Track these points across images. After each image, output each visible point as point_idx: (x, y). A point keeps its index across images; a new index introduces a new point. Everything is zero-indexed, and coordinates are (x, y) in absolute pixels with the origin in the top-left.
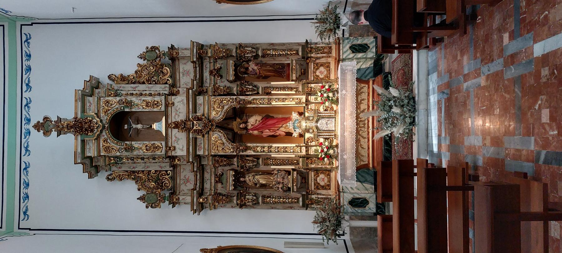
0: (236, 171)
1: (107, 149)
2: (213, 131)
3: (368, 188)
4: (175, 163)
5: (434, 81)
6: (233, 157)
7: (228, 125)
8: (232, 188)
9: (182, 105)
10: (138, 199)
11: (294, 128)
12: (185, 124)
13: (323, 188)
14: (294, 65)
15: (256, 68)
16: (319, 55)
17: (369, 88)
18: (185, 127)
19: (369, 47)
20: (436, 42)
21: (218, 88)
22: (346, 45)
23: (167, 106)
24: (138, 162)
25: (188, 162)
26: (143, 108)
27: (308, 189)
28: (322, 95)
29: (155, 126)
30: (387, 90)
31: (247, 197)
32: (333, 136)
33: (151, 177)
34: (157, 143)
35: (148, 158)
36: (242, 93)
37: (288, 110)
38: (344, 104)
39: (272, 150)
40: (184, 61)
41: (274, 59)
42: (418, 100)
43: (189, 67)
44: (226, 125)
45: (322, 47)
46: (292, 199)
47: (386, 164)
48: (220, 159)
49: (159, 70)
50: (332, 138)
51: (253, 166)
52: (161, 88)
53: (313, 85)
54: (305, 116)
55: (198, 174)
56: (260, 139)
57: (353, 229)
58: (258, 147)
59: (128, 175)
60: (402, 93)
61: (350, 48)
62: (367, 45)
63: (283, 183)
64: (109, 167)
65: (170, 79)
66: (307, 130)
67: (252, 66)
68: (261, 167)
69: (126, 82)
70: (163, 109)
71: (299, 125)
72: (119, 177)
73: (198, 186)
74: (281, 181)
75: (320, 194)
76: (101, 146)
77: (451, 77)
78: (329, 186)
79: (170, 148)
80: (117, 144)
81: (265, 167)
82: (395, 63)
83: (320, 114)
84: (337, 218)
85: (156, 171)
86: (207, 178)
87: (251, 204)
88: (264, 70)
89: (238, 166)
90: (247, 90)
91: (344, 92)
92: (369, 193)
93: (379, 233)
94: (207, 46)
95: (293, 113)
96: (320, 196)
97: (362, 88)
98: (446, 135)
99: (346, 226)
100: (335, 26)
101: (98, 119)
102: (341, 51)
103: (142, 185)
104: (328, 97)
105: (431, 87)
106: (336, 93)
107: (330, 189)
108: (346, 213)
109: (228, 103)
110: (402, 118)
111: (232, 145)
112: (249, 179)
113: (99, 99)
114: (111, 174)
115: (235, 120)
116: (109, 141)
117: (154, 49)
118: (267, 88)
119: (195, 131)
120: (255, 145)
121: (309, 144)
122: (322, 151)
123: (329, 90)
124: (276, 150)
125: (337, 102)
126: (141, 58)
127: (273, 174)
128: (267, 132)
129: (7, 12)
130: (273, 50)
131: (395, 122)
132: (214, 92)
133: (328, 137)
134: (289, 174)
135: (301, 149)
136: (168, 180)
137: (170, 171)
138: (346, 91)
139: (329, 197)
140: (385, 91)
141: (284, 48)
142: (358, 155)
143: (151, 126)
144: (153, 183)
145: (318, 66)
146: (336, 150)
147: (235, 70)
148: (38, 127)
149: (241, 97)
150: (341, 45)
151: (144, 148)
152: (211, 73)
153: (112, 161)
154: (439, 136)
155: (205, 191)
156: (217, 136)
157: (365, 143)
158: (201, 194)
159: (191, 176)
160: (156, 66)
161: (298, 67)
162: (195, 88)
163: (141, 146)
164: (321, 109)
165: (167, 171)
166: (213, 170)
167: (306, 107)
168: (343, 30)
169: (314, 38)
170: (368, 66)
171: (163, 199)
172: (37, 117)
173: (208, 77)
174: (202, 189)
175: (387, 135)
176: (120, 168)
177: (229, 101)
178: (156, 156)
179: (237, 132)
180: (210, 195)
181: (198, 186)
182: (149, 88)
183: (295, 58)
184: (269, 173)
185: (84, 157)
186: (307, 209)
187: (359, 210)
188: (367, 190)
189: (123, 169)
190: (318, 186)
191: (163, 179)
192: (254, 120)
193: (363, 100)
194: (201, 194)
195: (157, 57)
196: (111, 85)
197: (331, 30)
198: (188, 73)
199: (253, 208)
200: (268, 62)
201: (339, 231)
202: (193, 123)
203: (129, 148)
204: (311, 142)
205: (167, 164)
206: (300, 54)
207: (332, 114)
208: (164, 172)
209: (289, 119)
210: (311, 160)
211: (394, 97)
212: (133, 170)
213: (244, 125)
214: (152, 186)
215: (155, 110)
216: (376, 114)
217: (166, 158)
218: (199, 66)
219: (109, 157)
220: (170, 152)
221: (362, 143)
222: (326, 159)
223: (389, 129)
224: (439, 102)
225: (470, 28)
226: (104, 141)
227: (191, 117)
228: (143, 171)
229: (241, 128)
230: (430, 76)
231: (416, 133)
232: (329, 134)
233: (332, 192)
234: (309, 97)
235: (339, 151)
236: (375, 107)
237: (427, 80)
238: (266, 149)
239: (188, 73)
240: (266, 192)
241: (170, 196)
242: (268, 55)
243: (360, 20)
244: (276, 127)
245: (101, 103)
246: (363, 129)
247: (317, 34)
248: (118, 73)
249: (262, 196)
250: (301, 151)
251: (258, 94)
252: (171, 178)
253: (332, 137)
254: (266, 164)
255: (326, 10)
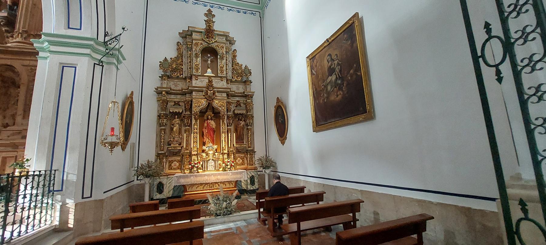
0: (182, 113)
1: (197, 44)
2: (206, 101)
3: (170, 192)
4: (187, 79)
5: (241, 224)
6: (191, 112)
7: (210, 109)
8: (171, 111)
9: (221, 85)
10: (166, 57)
11: (208, 147)
12: (211, 86)
13: (170, 165)
14: (244, 146)
15: (242, 125)
16: (249, 159)
17: (232, 188)
18: (209, 86)
19: (253, 186)
20: (264, 222)
21: (230, 105)
22: (254, 173)
23: (221, 77)
24: (189, 59)
25: (189, 87)
26: (220, 65)
27: (169, 156)
28: (228, 162)
29: (209, 70)
30: (235, 198)
31: (165, 120)
32: (204, 169)
33: (179, 66)
34: (200, 71)
35: (190, 65)
36: (228, 117)
37: (219, 142)
38: (224, 174)
39: (195, 135)
40: (244, 88)
41: (246, 135)
42: (230, 216)
43: (241, 90)
44: (209, 108)
45: (253, 160)
46: (163, 147)
47: (192, 202)
48: (189, 106)
49: (240, 75)
50: (203, 169)
51: (185, 123)
52: (230, 75)
53: (232, 156)
54: (216, 152)
55: (180, 92)
56: (201, 127)
57: (143, 186)
58: (197, 126)
59: (180, 54)
60: (234, 207)
61: (253, 176)
62: (254, 184)
63: (174, 141)
64: (185, 44)
65: (235, 80)
66: (207, 154)
67: (242, 123)
68: (184, 128)
69: (233, 58)
70: (219, 75)
71: (211, 149)
72: (179, 49)
73: (173, 91)
74: (175, 140)
75: (166, 164)
76: (199, 41)
77: (246, 233)
78: (171, 169)
79: (197, 77)
80: (200, 49)
81: (184, 130)
82: (247, 201)
83: (217, 161)
84: (151, 175)
85: (182, 69)
86: (177, 97)
87: (161, 122)
88: (241, 129)
89: (185, 114)
90: (230, 120)
91: (230, 174)
92: (166, 194)
93: (142, 203)
94: (252, 100)
95: (217, 146)
96: (165, 164)
97: (232, 184)
98: (213, 235)
99: (147, 180)
100: (265, 167)
101: (214, 41)
102: (251, 171)
103: (174, 60)
104: (228, 165)
105: (238, 223)
106: (229, 170)
107: (169, 169)
108: (153, 181)
109: (223, 110)
110: (220, 208)
111: (198, 111)
112: (177, 121)
113: (224, 43)
114: (181, 45)
115: (212, 113)
116: (201, 45)
117: (250, 73)
118: (231, 131)
119: (207, 91)
120: (198, 124)
121: (199, 156)
122: (195, 164)
123: (231, 165)
124: (195, 137)
125: (224, 170)
126: (245, 66)
127: (179, 135)
128: (206, 131)
129: (267, 7)
130: (251, 134)
131: (217, 205)
132: (228, 102)
133: (204, 167)
134: (179, 145)
135: (196, 151)
136: (177, 75)
137: (183, 76)
138: (231, 175)
139: (164, 170)
140: (235, 197)
141: (252, 140)
142: (193, 185)
143: (209, 68)
144: (175, 67)
145: (242, 159)
146: (196, 172)
147: (240, 114)
148: (209, 11)
149: (226, 117)
150: (254, 171)
151: (197, 63)
152: (238, 101)
153: (189, 46)
154: (211, 232)
155: (169, 95)
156: (204, 103)
157: (200, 188)
158: (167, 93)
159: (179, 88)
160: (241, 73)
161: (243, 148)
162: (231, 93)
163: (198, 62)
164: (220, 162)
165: (182, 74)
166: (182, 100)
167: (221, 153)
168: (262, 171)
169: (257, 156)
170: (243, 186)
171: (165, 71)
172: (215, 11)
173: (236, 100)
174: (171, 94)
175: (209, 201)
176: (185, 49)
177: (224, 110)
178: (192, 69)
179: (205, 114)
180: (167, 98)
181: (173, 91)
182: (230, 69)
183: (247, 146)
184: (180, 133)
185: (192, 32)
186: (155, 155)
187: (155, 189)
188: (169, 192)
189: (184, 51)
190: (171, 162)
191: (177, 72)
192: (213, 123)
193: (226, 185)
194: (167, 93)
195: (246, 74)
196: (231, 50)
197: (262, 164)
198: (238, 89)
199: (157, 123)
200: (244, 132)
201: (142, 177)
202: (212, 91)
203: (197, 55)
204: (200, 157)
205: (187, 74)
206: (249, 149)
207: (217, 168)
208: (182, 73)
209: (213, 144)
210: (188, 158)
211: (231, 203)
212: (183, 57)
213: (210, 118)
214: (173, 66)
215: (219, 71)
216: (222, 194)
217: (191, 75)
218: (242, 95)
219: (191, 45)
220: (195, 77)
221: (200, 187)
222: (190, 166)
223: (213, 202)
224: (231, 229)
225: (275, 239)
226: (201, 43)
227: (215, 89)
228: (182, 62)
229: (208, 116)
230: (243, 221)
231: (211, 218)
232: (205, 167)
233: (167, 171)
234: (226, 155)
235: (195, 174)
236: (225, 192)
237: (241, 220)
238: (196, 131)
239: (238, 89)
240: (168, 131)
241: (167, 75)
242: (248, 131)
243: (276, 180)
244: (209, 137)
245: (222, 44)
246: (209, 187)
247: (260, 157)
248: (237, 54)
249: (165, 129)
250: (194, 151)
251: (227, 126)
252: (178, 77)
253: (204, 169)
254: (185, 131)
255: (272, 161)
